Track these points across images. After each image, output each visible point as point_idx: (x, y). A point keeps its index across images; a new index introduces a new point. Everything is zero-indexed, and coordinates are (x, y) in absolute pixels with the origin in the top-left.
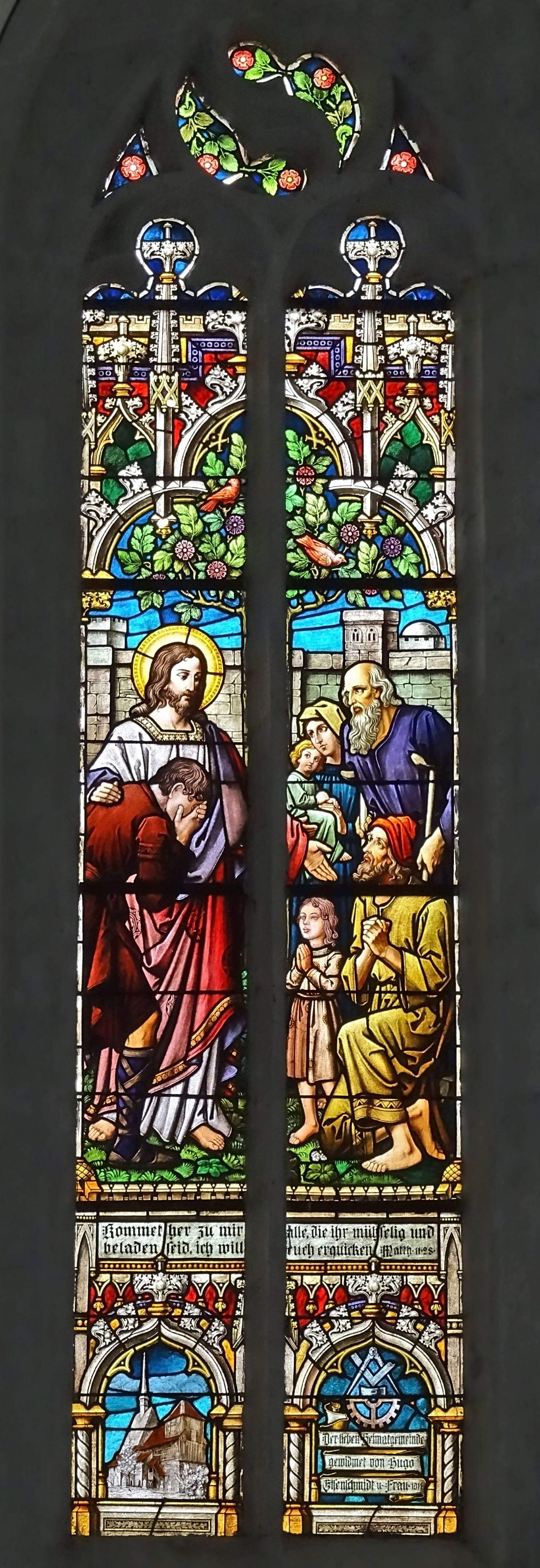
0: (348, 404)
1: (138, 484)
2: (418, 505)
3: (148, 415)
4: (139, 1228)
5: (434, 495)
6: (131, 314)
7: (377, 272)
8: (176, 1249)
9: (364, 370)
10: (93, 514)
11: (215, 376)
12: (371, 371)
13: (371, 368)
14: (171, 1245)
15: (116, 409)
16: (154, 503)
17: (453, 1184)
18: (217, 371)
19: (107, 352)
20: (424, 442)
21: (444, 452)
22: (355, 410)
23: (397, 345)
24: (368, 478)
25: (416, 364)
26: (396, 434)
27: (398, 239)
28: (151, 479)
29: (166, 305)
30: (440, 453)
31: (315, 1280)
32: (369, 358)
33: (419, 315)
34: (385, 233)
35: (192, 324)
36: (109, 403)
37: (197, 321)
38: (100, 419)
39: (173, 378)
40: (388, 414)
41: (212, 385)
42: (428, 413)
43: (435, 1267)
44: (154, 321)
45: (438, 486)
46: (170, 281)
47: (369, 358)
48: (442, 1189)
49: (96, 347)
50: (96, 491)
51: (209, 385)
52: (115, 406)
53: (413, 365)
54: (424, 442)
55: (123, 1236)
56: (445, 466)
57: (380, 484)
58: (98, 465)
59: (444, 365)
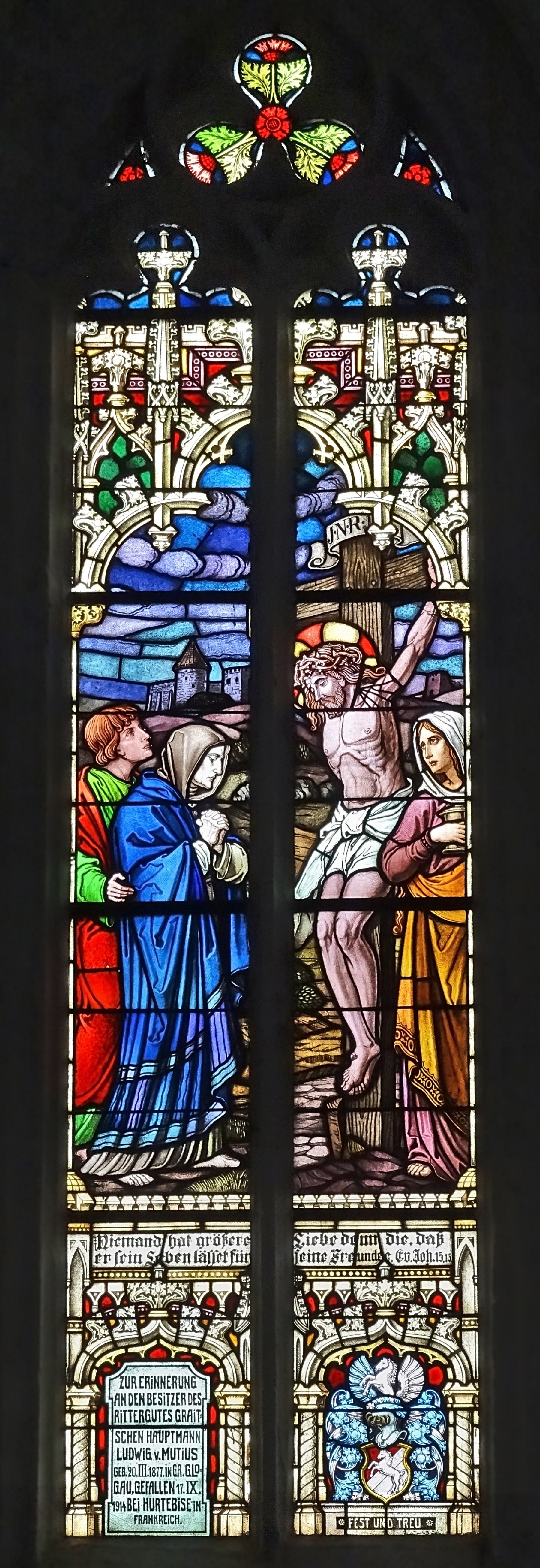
0: (358, 414)
1: (136, 496)
2: (430, 514)
3: (145, 426)
4: (146, 1239)
5: (448, 504)
6: (433, 320)
7: (168, 281)
8: (306, 1257)
9: (375, 378)
10: (86, 528)
11: (219, 387)
12: (165, 382)
13: (164, 378)
14: (216, 1254)
15: (110, 422)
16: (152, 516)
17: (468, 1190)
18: (221, 380)
19: (409, 360)
20: (436, 450)
21: (458, 460)
22: (364, 420)
23: (101, 357)
24: (378, 489)
25: (122, 376)
26: (406, 444)
27: (192, 250)
28: (149, 492)
29: (165, 314)
30: (453, 461)
31: (328, 1286)
32: (379, 366)
33: (431, 323)
34: (178, 244)
35: (194, 335)
36: (103, 414)
37: (200, 330)
38: (94, 431)
39: (390, 385)
40: (400, 424)
41: (215, 395)
42: (442, 421)
43: (451, 1271)
44: (152, 330)
45: (453, 494)
46: (167, 290)
47: (379, 366)
48: (458, 1195)
49: (90, 359)
50: (89, 503)
51: (211, 395)
52: (109, 418)
53: (118, 377)
54: (436, 450)
55: (177, 1247)
56: (459, 474)
57: (390, 494)
58: (93, 477)
59: (458, 373)
